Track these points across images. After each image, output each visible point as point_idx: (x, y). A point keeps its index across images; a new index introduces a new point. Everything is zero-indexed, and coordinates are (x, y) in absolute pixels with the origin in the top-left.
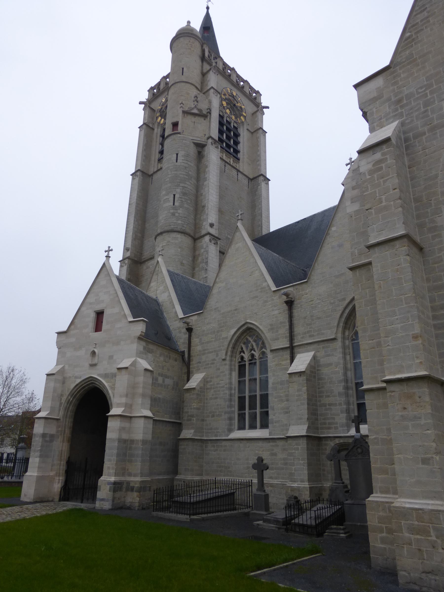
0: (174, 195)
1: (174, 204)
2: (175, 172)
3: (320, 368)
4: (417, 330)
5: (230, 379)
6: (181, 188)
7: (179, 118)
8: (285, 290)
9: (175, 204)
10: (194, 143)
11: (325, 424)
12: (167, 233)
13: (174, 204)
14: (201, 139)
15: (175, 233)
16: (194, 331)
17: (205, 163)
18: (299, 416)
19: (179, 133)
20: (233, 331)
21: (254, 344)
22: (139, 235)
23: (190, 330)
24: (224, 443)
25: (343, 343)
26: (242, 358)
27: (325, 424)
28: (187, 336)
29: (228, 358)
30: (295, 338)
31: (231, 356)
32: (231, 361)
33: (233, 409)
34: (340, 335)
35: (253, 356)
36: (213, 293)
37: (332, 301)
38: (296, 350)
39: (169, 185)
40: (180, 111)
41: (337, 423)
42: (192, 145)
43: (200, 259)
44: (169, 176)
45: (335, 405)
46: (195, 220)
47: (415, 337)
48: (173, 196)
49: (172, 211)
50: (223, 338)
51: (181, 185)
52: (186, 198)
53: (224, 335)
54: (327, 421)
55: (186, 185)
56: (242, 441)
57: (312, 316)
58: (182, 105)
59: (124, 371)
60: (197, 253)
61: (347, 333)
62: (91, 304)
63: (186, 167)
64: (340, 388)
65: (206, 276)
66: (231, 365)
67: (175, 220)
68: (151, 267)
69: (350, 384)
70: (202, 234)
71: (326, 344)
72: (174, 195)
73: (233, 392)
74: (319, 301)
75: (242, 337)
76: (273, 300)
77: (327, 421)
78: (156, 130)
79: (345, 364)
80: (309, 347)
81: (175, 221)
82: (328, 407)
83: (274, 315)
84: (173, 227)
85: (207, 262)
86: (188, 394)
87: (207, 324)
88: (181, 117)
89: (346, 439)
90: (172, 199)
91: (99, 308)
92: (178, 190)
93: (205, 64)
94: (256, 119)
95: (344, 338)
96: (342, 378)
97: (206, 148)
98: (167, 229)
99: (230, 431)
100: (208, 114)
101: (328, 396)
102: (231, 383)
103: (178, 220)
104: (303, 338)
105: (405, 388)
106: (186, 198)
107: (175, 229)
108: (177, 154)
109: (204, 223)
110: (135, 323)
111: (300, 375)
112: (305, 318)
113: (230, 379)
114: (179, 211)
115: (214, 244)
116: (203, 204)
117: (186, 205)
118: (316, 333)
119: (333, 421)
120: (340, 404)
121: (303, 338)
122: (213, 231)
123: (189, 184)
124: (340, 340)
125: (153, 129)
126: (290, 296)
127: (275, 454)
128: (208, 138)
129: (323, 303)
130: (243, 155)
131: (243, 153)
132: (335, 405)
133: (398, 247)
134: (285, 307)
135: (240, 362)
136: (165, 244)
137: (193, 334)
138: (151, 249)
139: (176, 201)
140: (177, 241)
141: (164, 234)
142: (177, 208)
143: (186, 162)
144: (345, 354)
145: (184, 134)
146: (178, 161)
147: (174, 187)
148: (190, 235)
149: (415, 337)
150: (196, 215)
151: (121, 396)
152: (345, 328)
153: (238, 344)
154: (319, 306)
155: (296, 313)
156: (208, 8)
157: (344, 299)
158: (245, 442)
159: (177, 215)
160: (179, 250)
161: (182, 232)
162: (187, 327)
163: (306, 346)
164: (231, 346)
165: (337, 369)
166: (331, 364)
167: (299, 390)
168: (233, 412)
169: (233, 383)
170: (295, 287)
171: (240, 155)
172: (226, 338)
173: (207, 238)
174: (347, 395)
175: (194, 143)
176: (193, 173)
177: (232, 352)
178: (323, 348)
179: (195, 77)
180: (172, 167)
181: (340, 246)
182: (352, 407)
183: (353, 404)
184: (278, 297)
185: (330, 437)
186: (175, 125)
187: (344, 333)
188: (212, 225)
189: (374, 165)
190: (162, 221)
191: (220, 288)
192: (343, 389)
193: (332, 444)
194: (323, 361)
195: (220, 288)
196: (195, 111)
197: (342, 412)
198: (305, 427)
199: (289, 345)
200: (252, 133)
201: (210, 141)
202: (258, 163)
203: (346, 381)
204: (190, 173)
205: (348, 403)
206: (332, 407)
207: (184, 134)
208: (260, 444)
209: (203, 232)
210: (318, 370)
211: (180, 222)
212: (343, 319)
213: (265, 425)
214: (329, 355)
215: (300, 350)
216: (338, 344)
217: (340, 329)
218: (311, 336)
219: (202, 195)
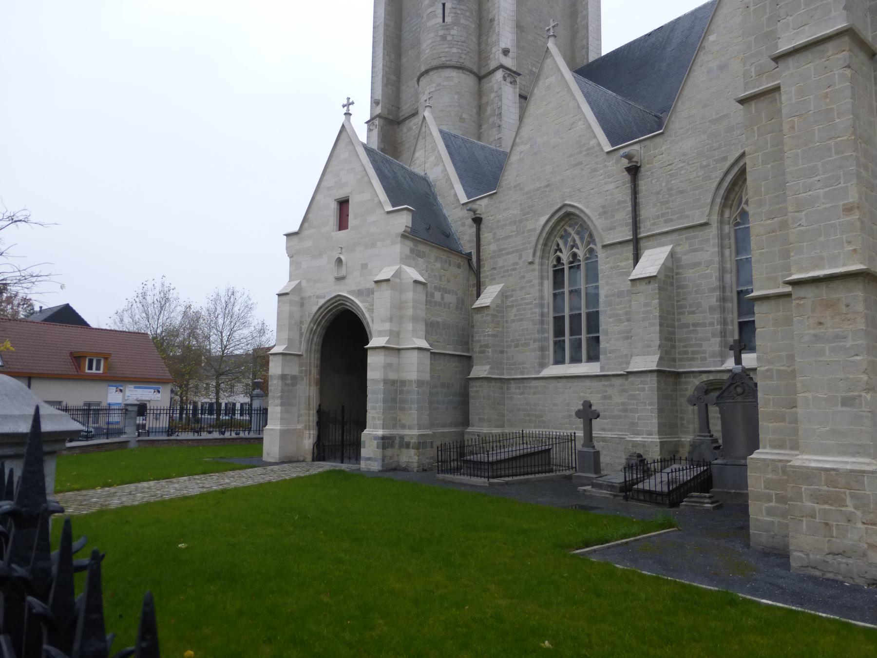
0: (444, 5)
1: (444, 21)
3: (680, 271)
8: (627, 150)
9: (446, 20)
11: (686, 353)
12: (436, 71)
13: (444, 21)
15: (449, 70)
16: (484, 221)
20: (543, 220)
21: (577, 237)
22: (393, 78)
23: (478, 221)
24: (534, 383)
25: (721, 229)
26: (559, 259)
29: (537, 260)
30: (642, 225)
31: (542, 257)
32: (542, 264)
33: (546, 335)
34: (715, 218)
35: (575, 255)
36: (511, 161)
37: (704, 163)
38: (642, 244)
41: (705, 352)
43: (489, 110)
45: (704, 325)
46: (479, 44)
48: (441, 6)
49: (441, 33)
52: (462, 7)
53: (530, 225)
54: (690, 350)
56: (559, 380)
57: (669, 189)
60: (484, 99)
61: (727, 214)
62: (329, 189)
64: (714, 301)
65: (500, 136)
66: (541, 271)
67: (446, 48)
71: (691, 233)
73: (546, 310)
75: (558, 228)
76: (606, 166)
79: (722, 261)
80: (664, 239)
81: (447, 50)
82: (691, 328)
83: (608, 191)
84: (443, 59)
85: (500, 114)
86: (480, 315)
89: (719, 374)
91: (341, 194)
95: (721, 222)
98: (435, 63)
99: (543, 365)
101: (693, 313)
102: (542, 298)
103: (451, 48)
104: (654, 224)
105: (823, 292)
106: (462, 7)
107: (448, 63)
109: (494, 50)
111: (650, 282)
112: (658, 193)
113: (541, 291)
115: (511, 83)
116: (490, 17)
117: (463, 21)
118: (676, 216)
119: (698, 349)
120: (712, 324)
121: (654, 224)
122: (508, 62)
126: (634, 160)
127: (610, 397)
129: (689, 167)
132: (704, 325)
133: (830, 52)
134: (627, 177)
135: (555, 266)
137: (483, 226)
138: (413, 99)
139: (446, 14)
140: (452, 83)
141: (431, 73)
142: (448, 27)
144: (722, 247)
148: (471, 72)
149: (849, 209)
150: (480, 36)
151: (383, 321)
152: (724, 206)
153: (552, 238)
154: (682, 172)
155: (644, 185)
157: (725, 159)
158: (565, 380)
159: (449, 38)
160: (456, 97)
162: (474, 217)
163: (659, 237)
164: (541, 242)
167: (647, 305)
170: (643, 144)
172: (534, 230)
173: (499, 74)
174: (723, 310)
177: (543, 251)
178: (687, 238)
181: (722, 67)
183: (732, 322)
184: (614, 161)
187: (721, 213)
188: (506, 52)
190: (428, 51)
191: (522, 152)
193: (696, 381)
194: (686, 259)
195: (522, 152)
197: (713, 335)
199: (632, 237)
205: (724, 323)
206: (698, 329)
208: (587, 383)
209: (493, 65)
211: (454, 50)
212: (722, 192)
213: (593, 357)
214: (695, 250)
217: (717, 208)
218: (666, 222)
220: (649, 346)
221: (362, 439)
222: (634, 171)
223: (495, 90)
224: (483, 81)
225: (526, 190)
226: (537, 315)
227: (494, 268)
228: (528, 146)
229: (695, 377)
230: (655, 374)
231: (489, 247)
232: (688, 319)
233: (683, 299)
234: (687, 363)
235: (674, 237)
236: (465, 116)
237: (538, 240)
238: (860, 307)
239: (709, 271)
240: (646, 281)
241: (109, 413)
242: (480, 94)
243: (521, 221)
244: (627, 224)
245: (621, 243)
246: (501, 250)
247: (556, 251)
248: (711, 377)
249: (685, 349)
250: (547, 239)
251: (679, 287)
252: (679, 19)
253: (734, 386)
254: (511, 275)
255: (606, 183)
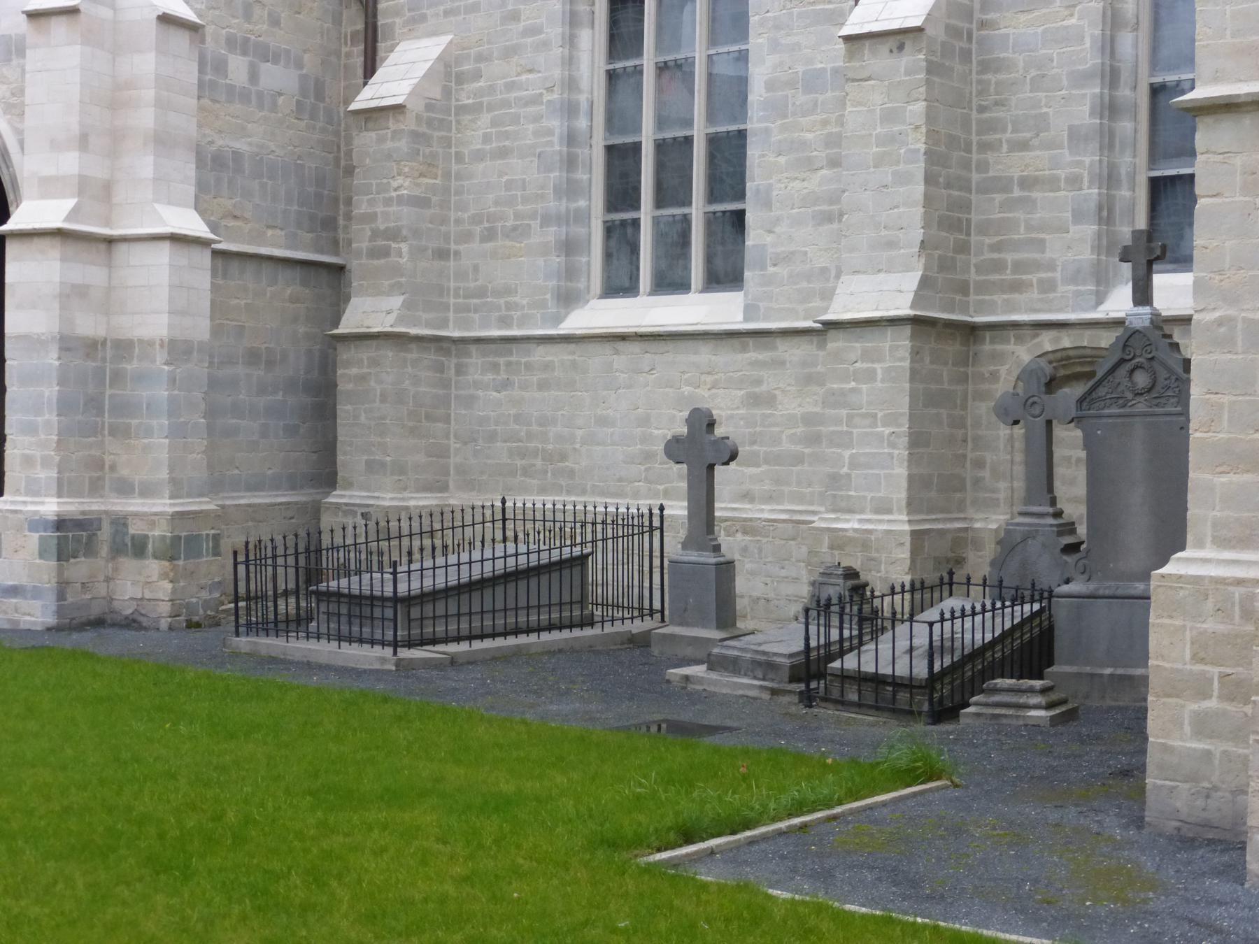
5: (570, 61)
11: (998, 266)
18: (884, 233)
24: (541, 354)
27: (998, 266)
41: (1051, 266)
54: (1009, 257)
59: (59, 27)
73: (582, 123)
82: (1017, 193)
99: (569, 299)
101: (1024, 146)
102: (571, 84)
111: (901, 47)
113: (570, 61)
119: (1037, 256)
120: (1074, 181)
165: (1073, 21)
167: (889, 116)
168: (582, 217)
169: (584, 84)
174: (1108, 141)
183: (1132, 177)
185: (1016, 325)
192: (1092, 114)
193: (1023, 353)
197: (1078, 217)
205: (1110, 178)
210: (983, 25)
226: (556, 139)
229: (1020, 340)
232: (1009, 164)
233: (997, 103)
234: (999, 298)
239: (1073, 21)
240: (892, 42)
249: (995, 256)
251: (985, 67)
253: (1129, 366)
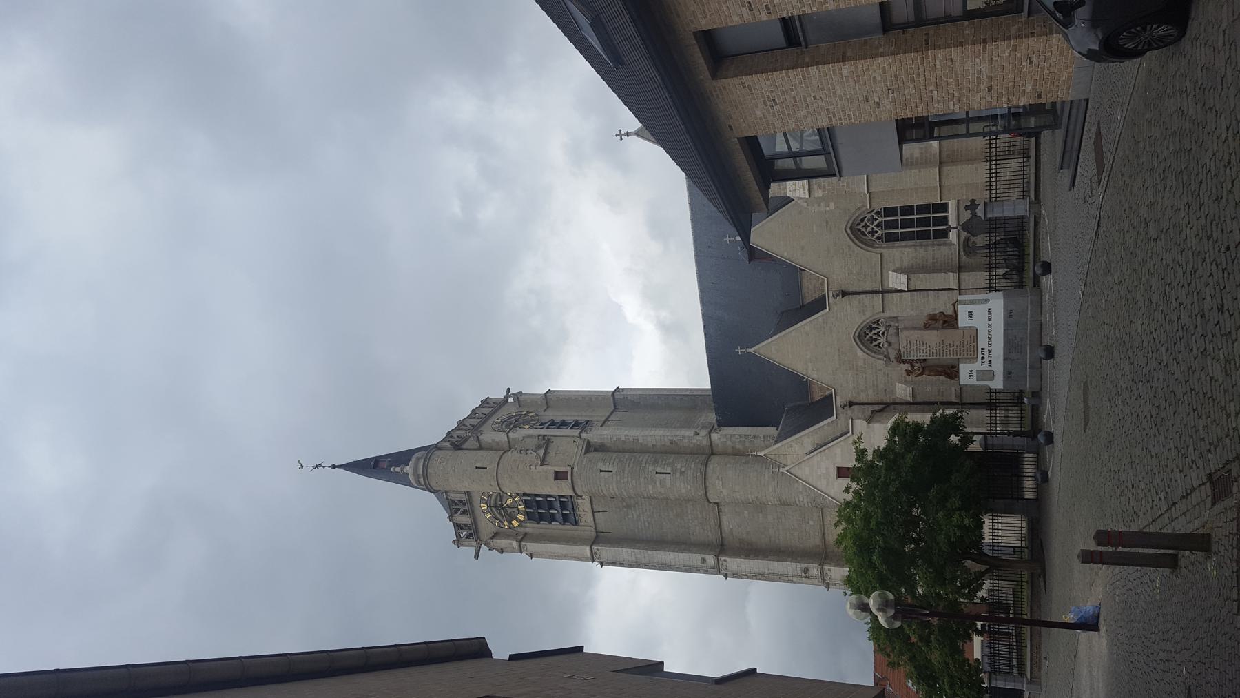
0: (657, 473)
1: (670, 473)
2: (626, 472)
4: (917, 171)
6: (647, 465)
7: (550, 469)
10: (585, 453)
11: (948, 263)
12: (707, 480)
13: (670, 473)
14: (582, 448)
16: (852, 400)
17: (613, 442)
19: (572, 469)
20: (860, 353)
23: (851, 404)
25: (884, 248)
28: (856, 407)
34: (878, 251)
38: (885, 288)
39: (642, 480)
40: (540, 468)
42: (586, 455)
43: (739, 446)
44: (630, 479)
47: (920, 171)
49: (678, 475)
50: (865, 364)
51: (644, 465)
52: (660, 460)
53: (861, 363)
54: (946, 261)
55: (644, 460)
57: (858, 274)
58: (533, 467)
60: (730, 451)
63: (620, 461)
64: (921, 250)
65: (762, 437)
68: (731, 527)
69: (918, 244)
70: (709, 444)
72: (657, 473)
74: (847, 268)
76: (836, 312)
77: (946, 261)
78: (527, 530)
80: (884, 274)
81: (692, 471)
84: (699, 474)
86: (918, 396)
87: (847, 383)
88: (550, 468)
90: (662, 475)
91: (834, 473)
92: (651, 468)
93: (466, 445)
94: (529, 401)
95: (881, 248)
96: (913, 249)
97: (591, 440)
100: (546, 438)
104: (876, 282)
106: (660, 460)
107: (702, 470)
108: (601, 471)
109: (694, 441)
110: (854, 429)
112: (859, 280)
114: (679, 467)
116: (668, 444)
117: (671, 460)
121: (876, 282)
123: (641, 458)
124: (882, 250)
125: (526, 533)
128: (580, 437)
130: (582, 416)
131: (578, 416)
136: (721, 482)
137: (855, 401)
139: (665, 471)
140: (718, 468)
141: (707, 484)
143: (612, 461)
144: (894, 247)
145: (574, 465)
146: (610, 470)
147: (646, 472)
148: (709, 457)
149: (920, 171)
156: (334, 467)
157: (849, 246)
159: (683, 469)
160: (728, 466)
161: (707, 464)
164: (873, 354)
166: (901, 258)
167: (922, 281)
171: (582, 419)
172: (865, 360)
174: (927, 245)
175: (585, 453)
176: (627, 455)
177: (879, 354)
179: (486, 458)
180: (619, 477)
181: (803, 249)
182: (935, 243)
186: (559, 476)
188: (696, 434)
189: (820, 189)
190: (689, 487)
191: (813, 370)
196: (541, 452)
197: (939, 249)
198: (951, 274)
200: (548, 407)
201: (584, 435)
202: (593, 400)
203: (915, 246)
204: (627, 457)
205: (933, 245)
207: (574, 465)
209: (705, 442)
210: (905, 269)
211: (693, 466)
212: (866, 247)
215: (886, 285)
216: (885, 251)
217: (873, 250)
219: (655, 446)
220: (945, 279)
221: (1002, 300)
222: (844, 294)
223: (725, 440)
224: (714, 452)
225: (838, 366)
227: (885, 390)
228: (810, 364)
230: (962, 274)
231: (870, 396)
235: (884, 271)
236: (743, 461)
237: (871, 356)
238: (949, 168)
241: (998, 536)
242: (725, 454)
243: (857, 370)
244: (873, 297)
245: (883, 302)
246: (873, 385)
247: (880, 347)
248: (962, 250)
250: (872, 351)
252: (703, 314)
254: (891, 378)
255: (846, 311)
